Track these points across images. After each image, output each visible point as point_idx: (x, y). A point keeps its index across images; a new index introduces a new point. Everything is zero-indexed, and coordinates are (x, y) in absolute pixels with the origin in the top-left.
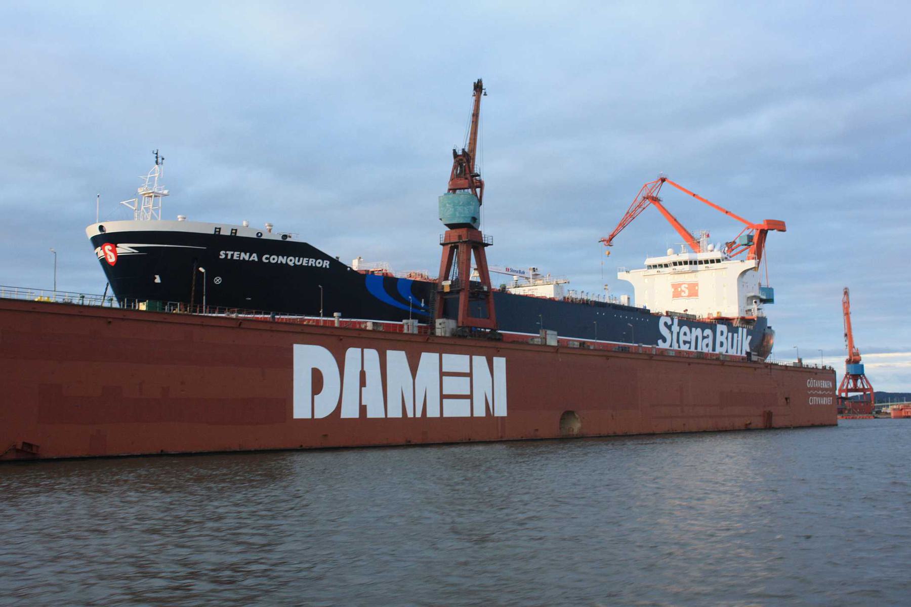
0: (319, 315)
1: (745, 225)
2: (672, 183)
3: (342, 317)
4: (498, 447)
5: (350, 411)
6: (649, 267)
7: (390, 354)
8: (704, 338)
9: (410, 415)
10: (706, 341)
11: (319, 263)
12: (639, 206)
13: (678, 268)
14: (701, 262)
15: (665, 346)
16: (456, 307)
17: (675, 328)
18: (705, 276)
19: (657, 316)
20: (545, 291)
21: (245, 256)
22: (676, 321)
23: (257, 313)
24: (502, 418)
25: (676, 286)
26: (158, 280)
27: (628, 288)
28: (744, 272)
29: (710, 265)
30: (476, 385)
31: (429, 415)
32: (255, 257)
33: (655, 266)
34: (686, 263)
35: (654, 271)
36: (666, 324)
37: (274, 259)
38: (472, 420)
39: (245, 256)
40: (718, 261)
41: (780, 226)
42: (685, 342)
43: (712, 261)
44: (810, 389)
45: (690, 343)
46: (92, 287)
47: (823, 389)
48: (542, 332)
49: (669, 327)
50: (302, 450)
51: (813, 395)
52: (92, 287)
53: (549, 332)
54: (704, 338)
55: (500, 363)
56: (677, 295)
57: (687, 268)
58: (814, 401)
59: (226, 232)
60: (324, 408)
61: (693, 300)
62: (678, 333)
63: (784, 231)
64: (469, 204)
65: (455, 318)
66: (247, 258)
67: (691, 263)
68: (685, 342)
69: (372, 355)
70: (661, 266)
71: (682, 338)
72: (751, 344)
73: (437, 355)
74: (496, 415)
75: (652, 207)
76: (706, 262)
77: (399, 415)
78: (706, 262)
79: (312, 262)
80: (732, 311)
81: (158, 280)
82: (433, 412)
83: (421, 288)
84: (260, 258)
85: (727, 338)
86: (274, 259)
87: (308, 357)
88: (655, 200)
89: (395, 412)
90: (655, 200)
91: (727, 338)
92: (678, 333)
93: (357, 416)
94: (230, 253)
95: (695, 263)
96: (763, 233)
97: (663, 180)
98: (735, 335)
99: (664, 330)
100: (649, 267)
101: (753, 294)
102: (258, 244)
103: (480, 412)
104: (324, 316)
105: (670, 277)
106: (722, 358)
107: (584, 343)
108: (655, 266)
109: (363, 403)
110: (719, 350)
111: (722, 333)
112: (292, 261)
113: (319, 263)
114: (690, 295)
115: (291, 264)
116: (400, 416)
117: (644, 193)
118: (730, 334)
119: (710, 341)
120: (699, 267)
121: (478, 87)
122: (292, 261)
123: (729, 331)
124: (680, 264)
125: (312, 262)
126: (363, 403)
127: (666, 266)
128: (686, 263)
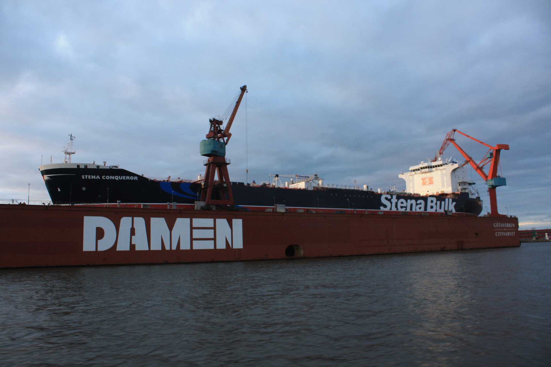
0: (106, 202)
1: (488, 148)
2: (459, 132)
3: (121, 202)
4: (240, 263)
5: (123, 246)
6: (411, 171)
7: (153, 220)
8: (417, 204)
9: (167, 248)
10: (418, 206)
11: (132, 178)
12: (445, 144)
13: (423, 170)
14: (434, 167)
15: (388, 209)
16: (216, 194)
17: (394, 200)
18: (436, 174)
19: (381, 195)
20: (301, 185)
21: (94, 177)
22: (394, 197)
23: (58, 203)
24: (239, 250)
25: (423, 179)
26: (59, 190)
27: (403, 182)
28: (454, 170)
29: (438, 168)
30: (229, 233)
31: (182, 248)
32: (98, 177)
33: (414, 171)
34: (426, 168)
35: (413, 173)
36: (386, 198)
37: (108, 178)
38: (215, 251)
39: (94, 177)
40: (441, 165)
41: (506, 147)
42: (402, 207)
43: (439, 166)
44: (496, 228)
45: (406, 207)
46: (41, 197)
47: (507, 228)
48: (275, 205)
49: (389, 200)
50: (89, 266)
51: (498, 231)
52: (41, 197)
53: (278, 205)
54: (417, 204)
55: (238, 223)
56: (424, 184)
57: (427, 170)
58: (499, 234)
59: (82, 167)
60: (105, 245)
61: (431, 186)
62: (396, 203)
63: (508, 149)
64: (211, 144)
65: (205, 201)
66: (95, 178)
67: (429, 167)
68: (402, 207)
69: (140, 222)
70: (416, 170)
71: (399, 205)
72: (455, 206)
73: (189, 220)
74: (234, 247)
75: (451, 144)
76: (436, 166)
77: (159, 248)
78: (436, 166)
79: (128, 178)
80: (448, 190)
81: (59, 190)
82: (185, 246)
83: (195, 186)
84: (101, 177)
85: (436, 204)
86: (108, 178)
87: (91, 223)
88: (452, 140)
89: (156, 246)
90: (452, 140)
91: (436, 204)
92: (396, 203)
93: (84, 250)
94: (86, 176)
95: (431, 167)
96: (498, 152)
97: (455, 130)
98: (443, 203)
99: (383, 201)
100: (411, 171)
101: (461, 181)
102: (98, 171)
103: (221, 245)
104: (109, 202)
105: (420, 175)
106: (423, 214)
107: (308, 210)
108: (414, 171)
109: (133, 243)
110: (429, 210)
111: (432, 202)
112: (117, 178)
113: (132, 178)
114: (429, 184)
115: (117, 179)
116: (160, 249)
117: (447, 138)
118: (438, 202)
119: (423, 206)
120: (434, 169)
121: (244, 89)
122: (117, 178)
123: (437, 200)
124: (424, 168)
125: (128, 178)
126: (133, 243)
127: (419, 170)
128: (426, 168)
